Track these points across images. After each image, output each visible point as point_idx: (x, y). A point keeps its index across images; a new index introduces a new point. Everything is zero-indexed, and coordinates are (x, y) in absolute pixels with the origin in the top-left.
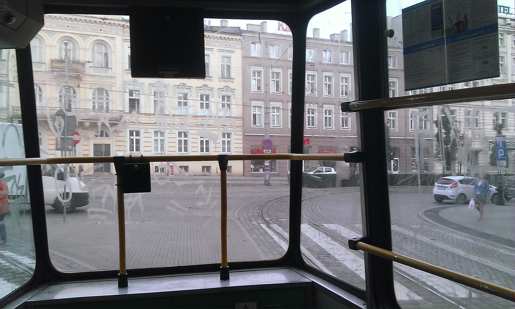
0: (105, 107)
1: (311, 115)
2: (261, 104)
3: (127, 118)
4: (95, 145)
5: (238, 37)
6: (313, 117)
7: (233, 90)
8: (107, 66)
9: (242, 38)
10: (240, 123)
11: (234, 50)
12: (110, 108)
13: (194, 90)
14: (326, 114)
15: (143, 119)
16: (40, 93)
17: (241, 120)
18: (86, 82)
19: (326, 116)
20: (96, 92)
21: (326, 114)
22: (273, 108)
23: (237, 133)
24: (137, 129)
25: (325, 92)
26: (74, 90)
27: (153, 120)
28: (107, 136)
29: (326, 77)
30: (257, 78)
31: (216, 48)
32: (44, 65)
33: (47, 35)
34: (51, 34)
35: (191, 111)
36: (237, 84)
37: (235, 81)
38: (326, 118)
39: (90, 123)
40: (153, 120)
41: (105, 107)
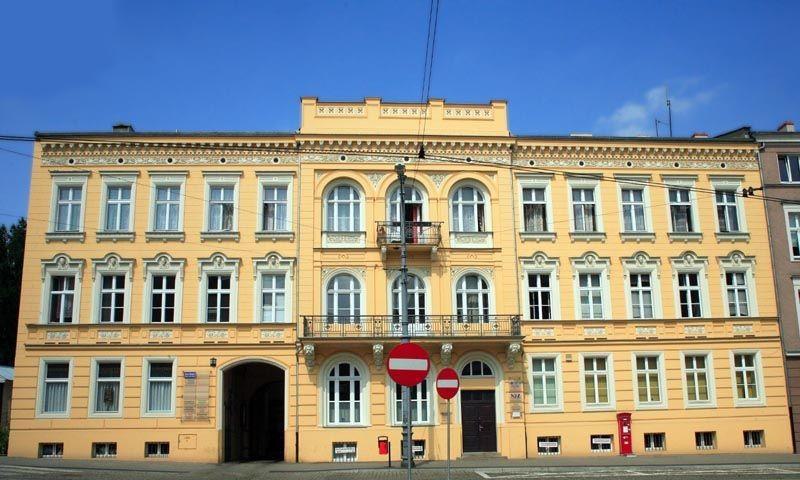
3: (529, 332)
5: (748, 148)
7: (748, 259)
13: (249, 266)
23: (769, 352)
24: (601, 354)
26: (356, 280)
28: (488, 371)
41: (352, 313)
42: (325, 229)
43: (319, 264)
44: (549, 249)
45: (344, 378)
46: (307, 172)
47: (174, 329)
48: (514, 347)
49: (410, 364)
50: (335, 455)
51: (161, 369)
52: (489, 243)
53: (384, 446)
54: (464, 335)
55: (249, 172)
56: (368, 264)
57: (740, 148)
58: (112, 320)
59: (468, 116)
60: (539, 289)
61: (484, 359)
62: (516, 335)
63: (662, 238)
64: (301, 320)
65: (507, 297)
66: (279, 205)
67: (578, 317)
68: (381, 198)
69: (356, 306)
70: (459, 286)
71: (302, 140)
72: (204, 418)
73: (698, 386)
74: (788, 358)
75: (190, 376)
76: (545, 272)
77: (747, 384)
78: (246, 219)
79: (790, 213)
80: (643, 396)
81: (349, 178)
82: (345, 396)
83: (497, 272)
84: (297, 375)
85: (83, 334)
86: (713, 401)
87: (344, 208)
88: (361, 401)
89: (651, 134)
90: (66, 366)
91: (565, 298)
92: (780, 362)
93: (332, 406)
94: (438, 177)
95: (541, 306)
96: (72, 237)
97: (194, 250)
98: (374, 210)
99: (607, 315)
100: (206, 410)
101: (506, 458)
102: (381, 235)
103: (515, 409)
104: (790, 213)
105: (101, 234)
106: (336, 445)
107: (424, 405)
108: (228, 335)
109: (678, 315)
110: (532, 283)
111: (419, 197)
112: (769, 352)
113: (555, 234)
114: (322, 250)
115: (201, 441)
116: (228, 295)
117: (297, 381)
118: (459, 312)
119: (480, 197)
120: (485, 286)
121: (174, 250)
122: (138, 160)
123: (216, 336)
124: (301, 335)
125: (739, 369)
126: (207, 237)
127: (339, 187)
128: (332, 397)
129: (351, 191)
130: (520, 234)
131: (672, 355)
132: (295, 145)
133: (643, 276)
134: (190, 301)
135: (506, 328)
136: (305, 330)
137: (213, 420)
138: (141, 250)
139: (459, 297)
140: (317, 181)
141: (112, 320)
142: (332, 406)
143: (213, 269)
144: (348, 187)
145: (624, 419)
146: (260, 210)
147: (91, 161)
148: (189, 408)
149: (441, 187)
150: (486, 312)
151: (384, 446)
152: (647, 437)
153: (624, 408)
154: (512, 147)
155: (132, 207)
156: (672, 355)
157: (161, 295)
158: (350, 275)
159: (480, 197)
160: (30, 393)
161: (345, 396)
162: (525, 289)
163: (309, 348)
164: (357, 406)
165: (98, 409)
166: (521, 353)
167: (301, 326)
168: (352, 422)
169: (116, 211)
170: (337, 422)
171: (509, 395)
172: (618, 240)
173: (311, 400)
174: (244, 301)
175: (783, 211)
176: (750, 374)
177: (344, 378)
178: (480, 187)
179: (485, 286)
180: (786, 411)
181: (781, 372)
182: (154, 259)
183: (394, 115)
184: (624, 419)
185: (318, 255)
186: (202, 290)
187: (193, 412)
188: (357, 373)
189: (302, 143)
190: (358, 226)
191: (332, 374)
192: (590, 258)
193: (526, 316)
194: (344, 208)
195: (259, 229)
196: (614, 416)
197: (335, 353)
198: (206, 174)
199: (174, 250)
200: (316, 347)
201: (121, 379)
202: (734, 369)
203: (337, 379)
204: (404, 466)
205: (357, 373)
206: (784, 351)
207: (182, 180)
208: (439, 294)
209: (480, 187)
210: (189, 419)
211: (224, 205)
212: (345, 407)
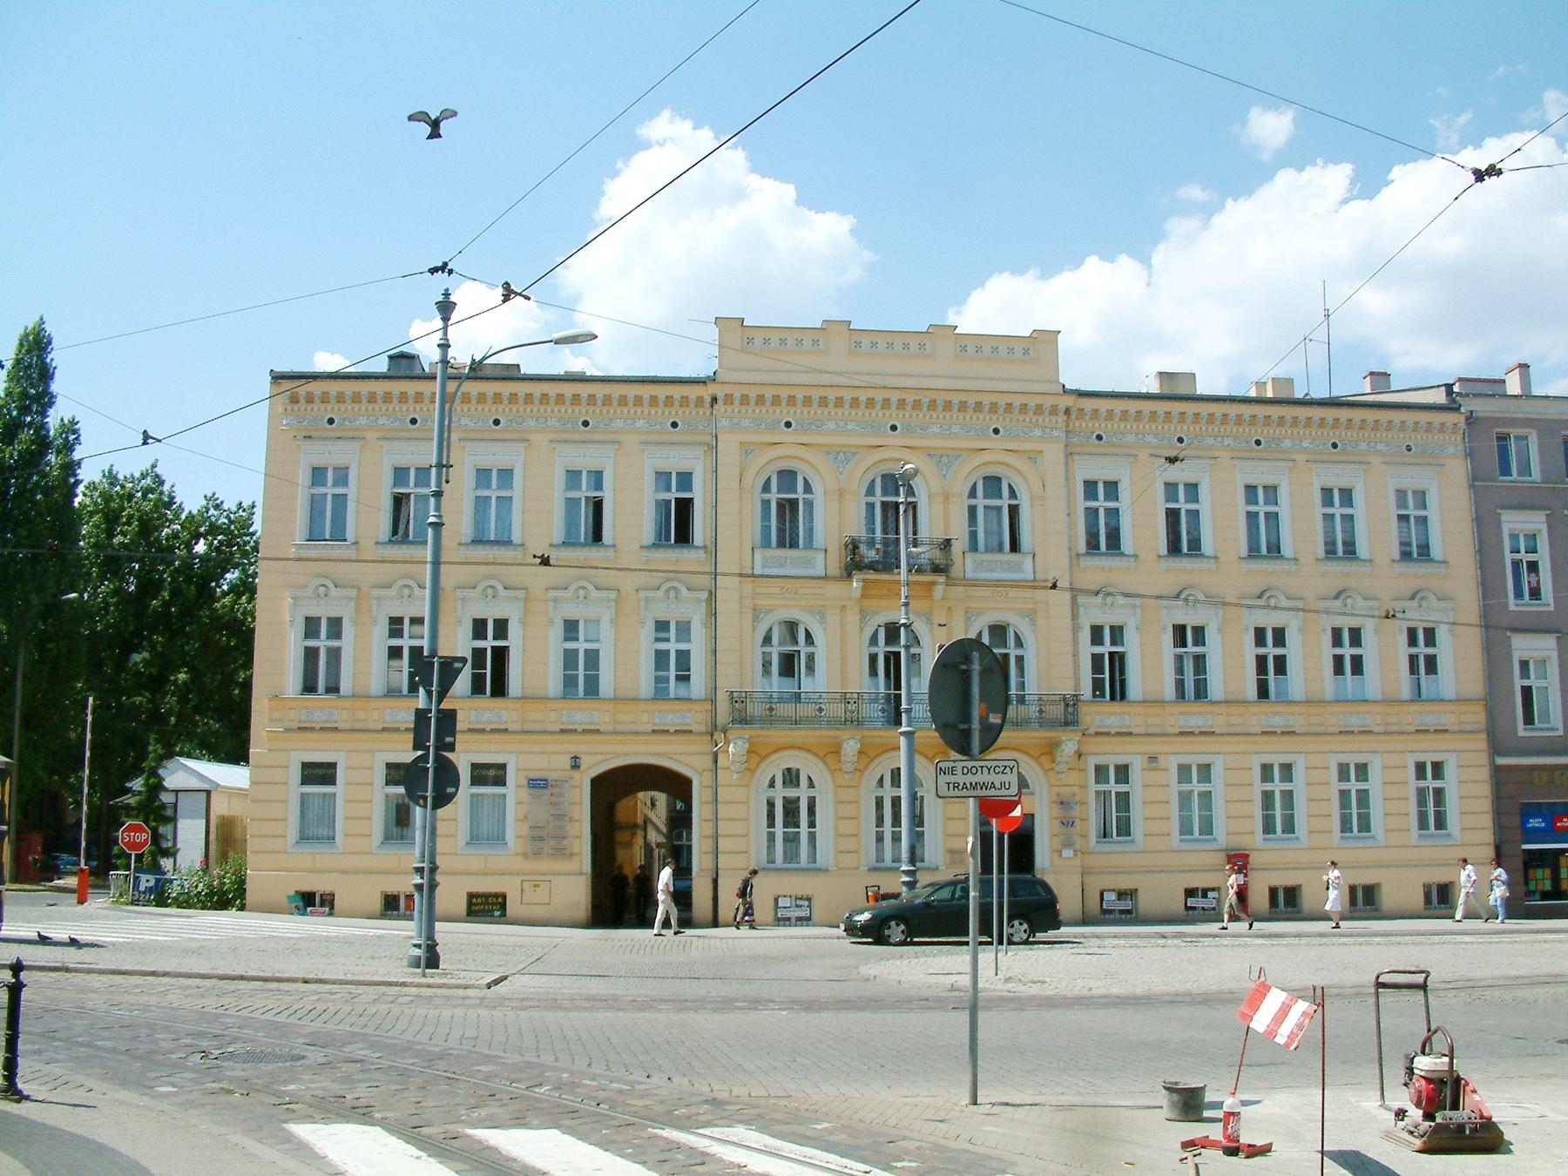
50: (1187, 908)
60: (1271, 651)
69: (1197, 672)
72: (561, 852)
75: (537, 784)
80: (1268, 828)
81: (1007, 465)
88: (818, 829)
90: (333, 766)
93: (771, 838)
100: (565, 842)
103: (1068, 844)
106: (1190, 893)
109: (1170, 691)
113: (1216, 558)
116: (688, 652)
125: (1344, 786)
128: (771, 824)
146: (387, 505)
154: (1067, 411)
155: (351, 498)
164: (812, 838)
171: (1056, 823)
175: (1499, 526)
176: (1439, 792)
185: (748, 586)
188: (811, 785)
191: (772, 784)
193: (1086, 689)
196: (1222, 857)
197: (778, 750)
205: (811, 785)
210: (538, 854)
212: (791, 840)
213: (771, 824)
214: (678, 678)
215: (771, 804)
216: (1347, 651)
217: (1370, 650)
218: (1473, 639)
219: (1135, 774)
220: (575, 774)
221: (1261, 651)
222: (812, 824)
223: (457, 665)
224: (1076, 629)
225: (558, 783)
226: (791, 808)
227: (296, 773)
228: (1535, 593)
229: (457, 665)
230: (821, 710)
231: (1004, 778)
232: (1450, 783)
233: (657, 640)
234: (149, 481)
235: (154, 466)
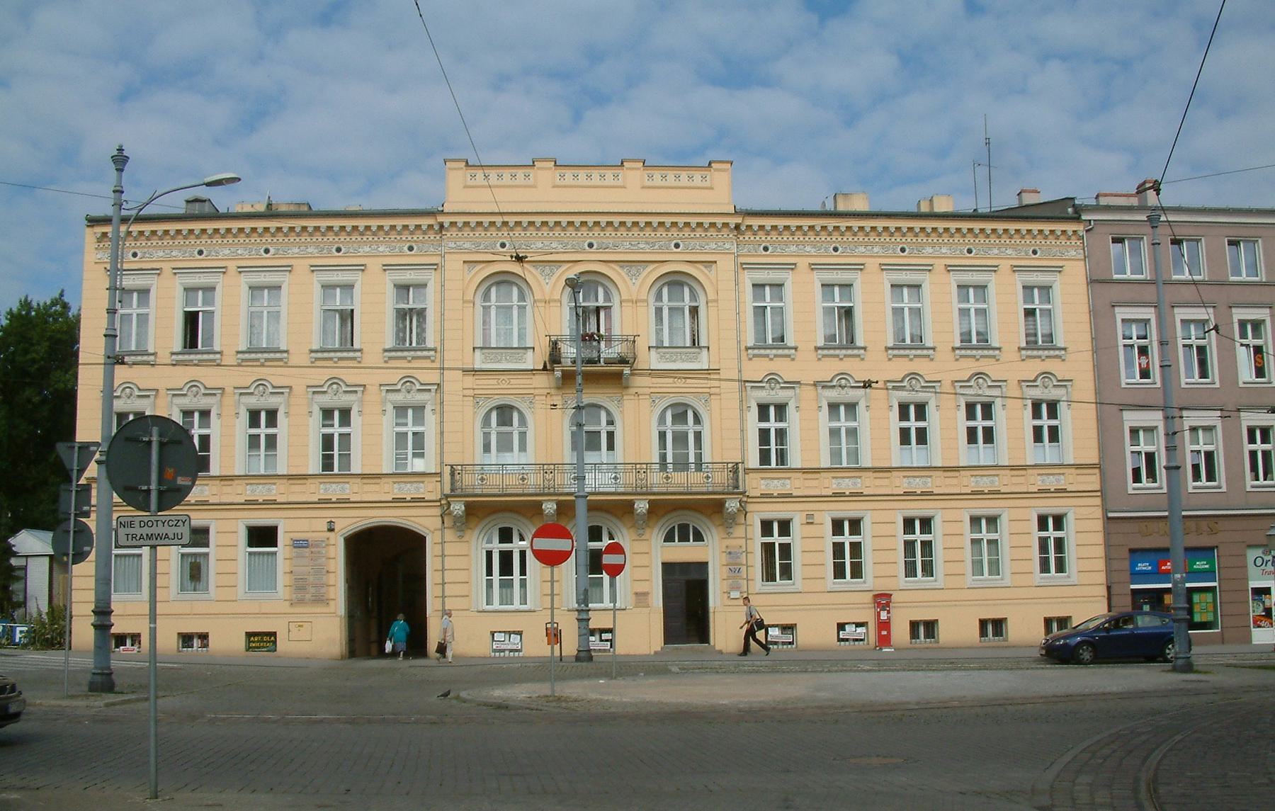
0: (692, 459)
1: (1259, 447)
2: (1212, 418)
3: (755, 484)
4: (668, 568)
5: (1070, 227)
6: (1266, 454)
7: (1063, 383)
8: (695, 342)
9: (1080, 228)
10: (1092, 481)
11: (1060, 263)
12: (706, 458)
13: (373, 394)
14: (1252, 440)
15: (798, 483)
16: (522, 429)
17: (1097, 471)
18: (640, 391)
19: (1253, 447)
20: (494, 415)
21: (1252, 440)
22: (1194, 429)
23: (1084, 512)
24: (926, 513)
25: (1246, 373)
26: (609, 413)
27: (830, 484)
28: (699, 537)
29: (1243, 324)
30: (1250, 340)
31: (1005, 265)
32: (530, 352)
33: (623, 272)
34: (634, 270)
35: (936, 453)
36: (1077, 368)
37: (1004, 356)
38: (1253, 454)
39: (650, 502)
40: (830, 484)
41: (692, 459)
42: (479, 344)
43: (471, 392)
44: (994, 370)
45: (506, 546)
46: (454, 264)
47: (352, 480)
48: (732, 505)
49: (574, 528)
50: (840, 640)
51: (263, 536)
52: (703, 362)
53: (554, 635)
54: (613, 490)
55: (301, 266)
56: (536, 392)
57: (1058, 227)
58: (773, 465)
59: (663, 183)
61: (694, 520)
62: (735, 488)
63: (944, 354)
64: (447, 470)
65: (728, 436)
66: (519, 307)
67: (825, 462)
68: (555, 301)
70: (662, 419)
71: (446, 220)
72: (320, 600)
73: (987, 557)
74: (1108, 520)
75: (299, 544)
76: (271, 407)
77: (1053, 556)
78: (376, 328)
79: (1123, 320)
80: (910, 571)
82: (506, 568)
83: (714, 402)
84: (443, 543)
85: (226, 489)
86: (1007, 576)
87: (505, 311)
89: (967, 206)
91: (808, 436)
92: (1098, 525)
93: (490, 584)
94: (547, 270)
95: (772, 449)
96: (139, 358)
97: (946, 368)
98: (553, 318)
99: (866, 461)
100: (323, 590)
101: (720, 652)
102: (555, 357)
104: (1123, 320)
105: (316, 351)
107: (523, 584)
108: (352, 490)
110: (763, 416)
111: (608, 297)
112: (1084, 512)
114: (475, 371)
115: (317, 628)
117: (443, 550)
118: (663, 457)
119: (694, 296)
120: (697, 420)
121: (276, 376)
122: (224, 252)
123: (334, 490)
124: (447, 491)
126: (320, 355)
127: (669, 284)
128: (489, 572)
129: (686, 290)
130: (747, 349)
131: (1018, 514)
132: (436, 228)
133: (1048, 405)
134: (299, 441)
135: (721, 478)
136: (452, 484)
137: (332, 603)
138: (878, 366)
139: (662, 436)
140: (468, 277)
141: (773, 465)
142: (490, 584)
143: (327, 400)
144: (681, 284)
145: (882, 600)
147: (161, 254)
148: (299, 586)
149: (638, 283)
150: (699, 457)
151: (554, 635)
152: (914, 625)
153: (883, 586)
154: (737, 227)
155: (152, 318)
156: (1018, 514)
157: (976, 428)
158: (600, 407)
159: (694, 296)
160: (1085, 552)
161: (506, 568)
162: (753, 425)
163: (458, 508)
164: (523, 584)
165: (183, 589)
166: (743, 510)
167: (447, 477)
168: (517, 605)
169: (262, 318)
170: (496, 605)
171: (725, 569)
172: (883, 356)
173: (461, 576)
174: (372, 442)
177: (506, 546)
178: (524, 286)
179: (697, 420)
180: (1103, 591)
181: (1099, 538)
182: (968, 381)
183: (573, 183)
184: (882, 600)
186: (314, 429)
187: (306, 592)
189: (446, 225)
190: (424, 341)
192: (981, 381)
193: (753, 460)
194: (505, 311)
195: (390, 342)
196: (868, 597)
197: (675, 510)
198: (314, 269)
199: (276, 376)
200: (468, 506)
201: (211, 550)
202: (902, 537)
203: (497, 547)
204: (578, 659)
206: (1105, 510)
207: (357, 278)
208: (636, 426)
209: (524, 286)
210: (301, 602)
211: (341, 312)
212: (507, 585)
213: (489, 572)
214: (415, 455)
215: (489, 554)
216: (1045, 422)
217: (934, 421)
218: (1089, 414)
219: (795, 527)
220: (331, 534)
221: (1038, 422)
222: (523, 572)
223: (93, 448)
224: (743, 409)
225: (317, 544)
226: (506, 558)
227: (243, 536)
228: (1145, 374)
229: (93, 448)
230: (708, 477)
231: (176, 530)
232: (1070, 532)
233: (397, 424)
234: (58, 308)
235: (62, 295)
